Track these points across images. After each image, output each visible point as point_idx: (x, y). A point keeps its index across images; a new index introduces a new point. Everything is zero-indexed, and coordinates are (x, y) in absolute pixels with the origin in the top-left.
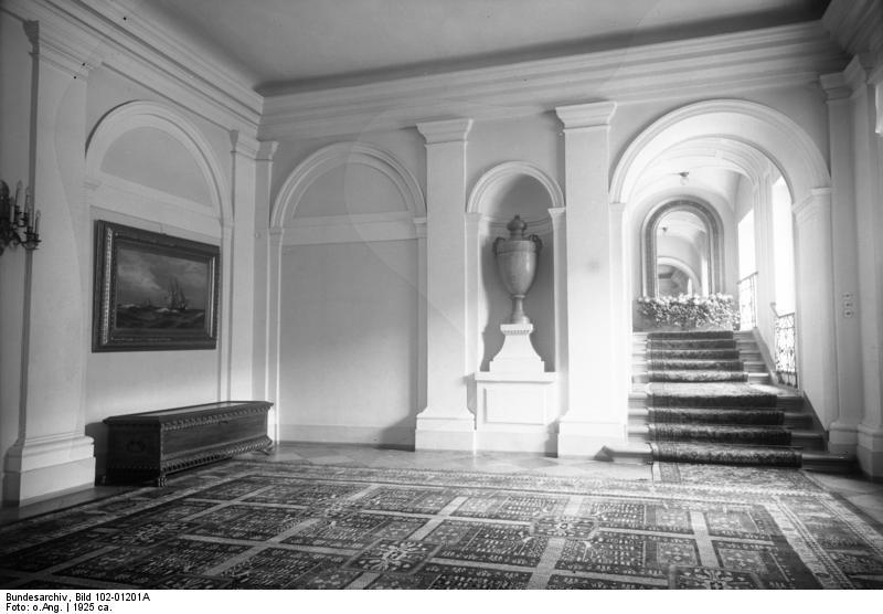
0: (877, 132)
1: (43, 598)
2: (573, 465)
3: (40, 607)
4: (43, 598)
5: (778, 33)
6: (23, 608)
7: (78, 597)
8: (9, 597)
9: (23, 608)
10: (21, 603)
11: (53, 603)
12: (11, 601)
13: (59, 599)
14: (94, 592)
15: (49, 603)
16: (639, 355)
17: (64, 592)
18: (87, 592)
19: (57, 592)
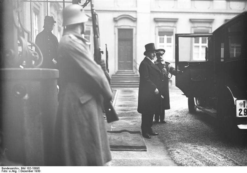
1: (12, 169)
3: (11, 171)
4: (12, 169)
6: (7, 171)
7: (22, 168)
8: (2, 168)
9: (7, 171)
10: (6, 170)
11: (15, 170)
13: (17, 169)
14: (26, 167)
15: (14, 170)
17: (18, 167)
18: (24, 167)
19: (16, 167)
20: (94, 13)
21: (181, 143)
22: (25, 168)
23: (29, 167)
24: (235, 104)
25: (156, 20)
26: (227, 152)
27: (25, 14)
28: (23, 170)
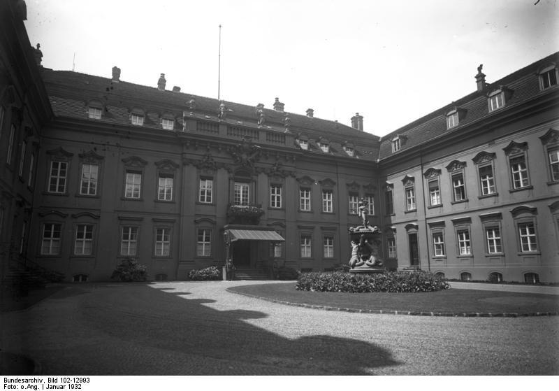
1: (27, 381)
3: (26, 387)
4: (27, 381)
7: (49, 380)
8: (5, 380)
9: (15, 387)
10: (13, 384)
11: (34, 384)
12: (7, 383)
13: (37, 381)
14: (59, 377)
15: (31, 384)
17: (40, 377)
18: (55, 377)
19: (36, 377)
22: (56, 381)
23: (67, 377)
25: (432, 225)
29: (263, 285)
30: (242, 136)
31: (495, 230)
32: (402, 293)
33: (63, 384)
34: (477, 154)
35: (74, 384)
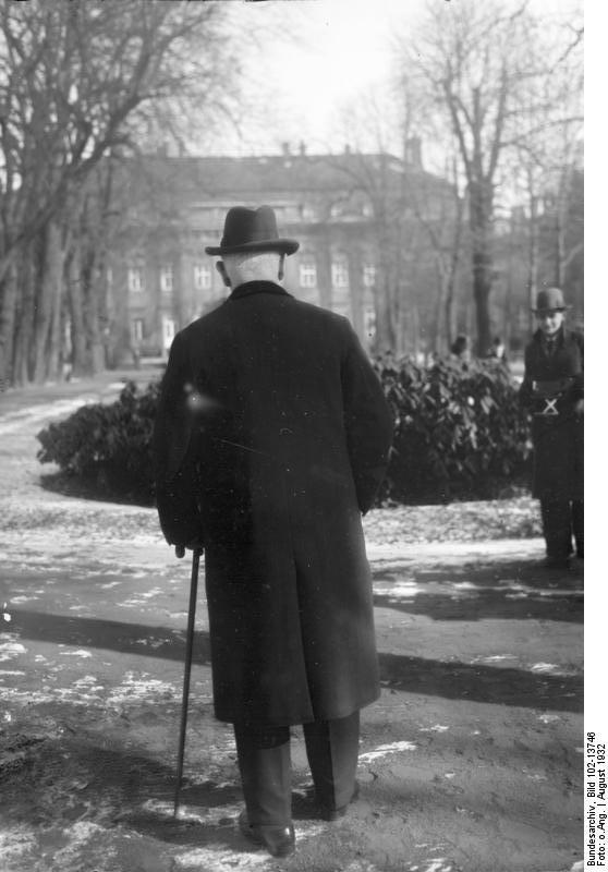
0: (192, 552)
1: (593, 830)
2: (36, 554)
4: (593, 830)
5: (486, 748)
7: (591, 795)
8: (591, 864)
10: (597, 851)
11: (597, 819)
12: (596, 861)
13: (593, 814)
14: (587, 780)
15: (597, 823)
16: (216, 40)
17: (587, 809)
18: (586, 786)
19: (586, 815)
20: (123, 130)
21: (448, 582)
22: (592, 784)
23: (586, 768)
24: (411, 602)
26: (439, 819)
27: (486, 556)
28: (597, 792)
29: (10, 670)
30: (102, 537)
31: (105, 690)
32: (213, 229)
33: (597, 774)
34: (79, 403)
35: (596, 755)
